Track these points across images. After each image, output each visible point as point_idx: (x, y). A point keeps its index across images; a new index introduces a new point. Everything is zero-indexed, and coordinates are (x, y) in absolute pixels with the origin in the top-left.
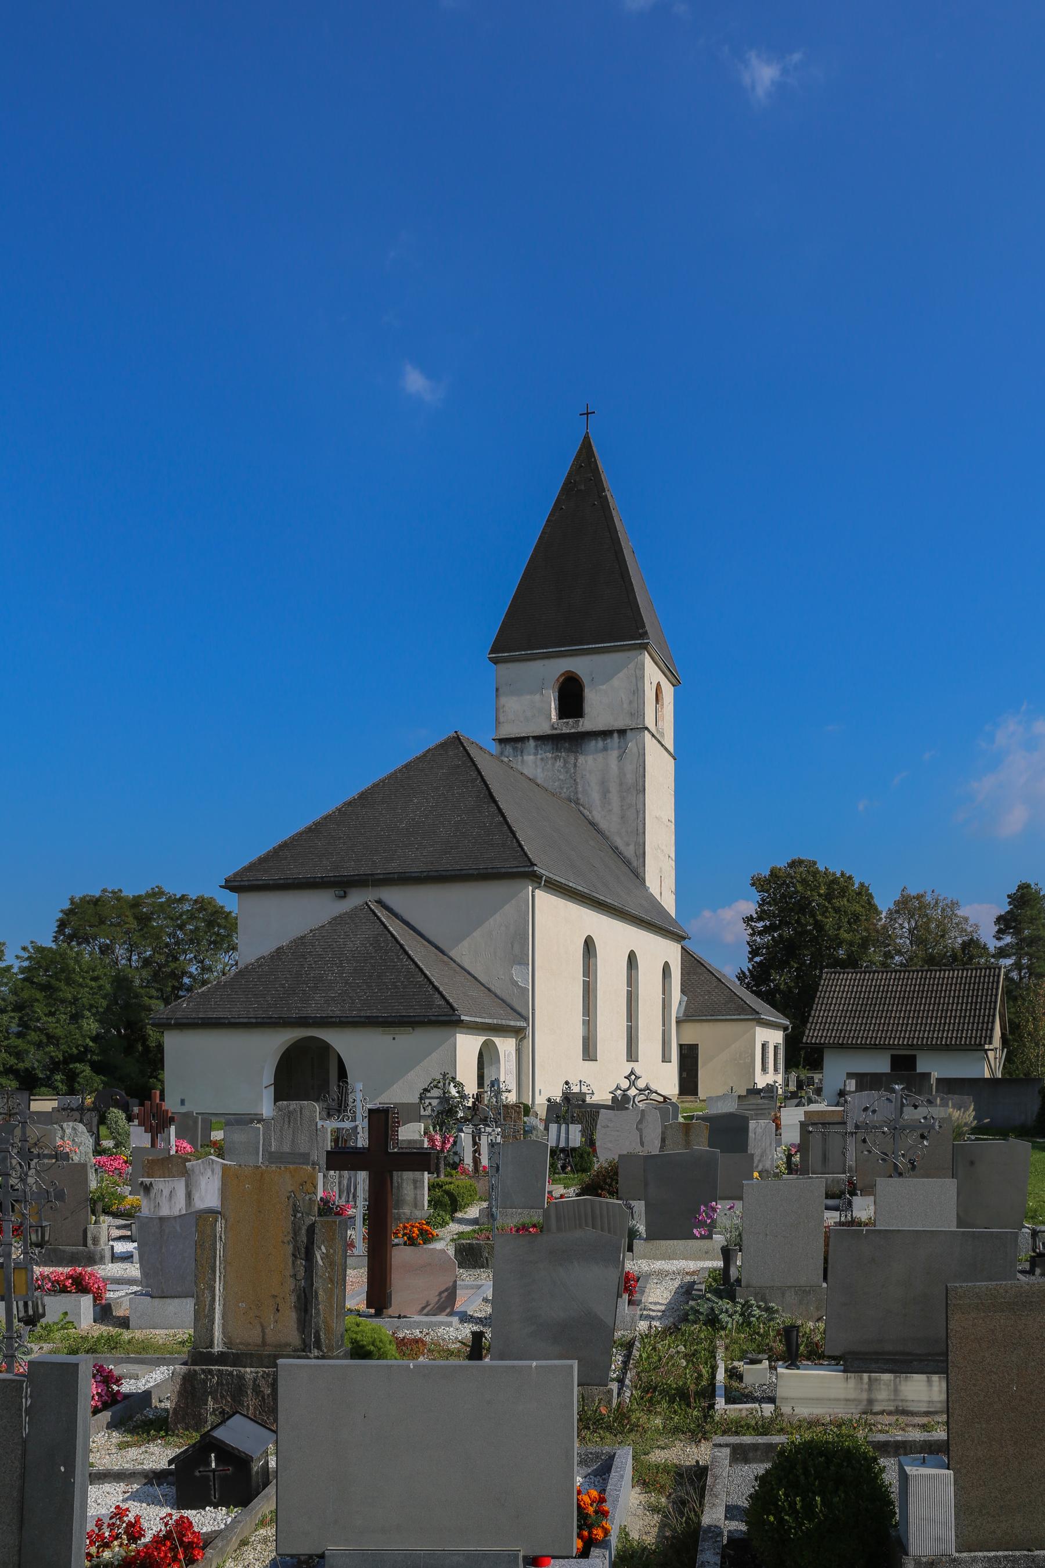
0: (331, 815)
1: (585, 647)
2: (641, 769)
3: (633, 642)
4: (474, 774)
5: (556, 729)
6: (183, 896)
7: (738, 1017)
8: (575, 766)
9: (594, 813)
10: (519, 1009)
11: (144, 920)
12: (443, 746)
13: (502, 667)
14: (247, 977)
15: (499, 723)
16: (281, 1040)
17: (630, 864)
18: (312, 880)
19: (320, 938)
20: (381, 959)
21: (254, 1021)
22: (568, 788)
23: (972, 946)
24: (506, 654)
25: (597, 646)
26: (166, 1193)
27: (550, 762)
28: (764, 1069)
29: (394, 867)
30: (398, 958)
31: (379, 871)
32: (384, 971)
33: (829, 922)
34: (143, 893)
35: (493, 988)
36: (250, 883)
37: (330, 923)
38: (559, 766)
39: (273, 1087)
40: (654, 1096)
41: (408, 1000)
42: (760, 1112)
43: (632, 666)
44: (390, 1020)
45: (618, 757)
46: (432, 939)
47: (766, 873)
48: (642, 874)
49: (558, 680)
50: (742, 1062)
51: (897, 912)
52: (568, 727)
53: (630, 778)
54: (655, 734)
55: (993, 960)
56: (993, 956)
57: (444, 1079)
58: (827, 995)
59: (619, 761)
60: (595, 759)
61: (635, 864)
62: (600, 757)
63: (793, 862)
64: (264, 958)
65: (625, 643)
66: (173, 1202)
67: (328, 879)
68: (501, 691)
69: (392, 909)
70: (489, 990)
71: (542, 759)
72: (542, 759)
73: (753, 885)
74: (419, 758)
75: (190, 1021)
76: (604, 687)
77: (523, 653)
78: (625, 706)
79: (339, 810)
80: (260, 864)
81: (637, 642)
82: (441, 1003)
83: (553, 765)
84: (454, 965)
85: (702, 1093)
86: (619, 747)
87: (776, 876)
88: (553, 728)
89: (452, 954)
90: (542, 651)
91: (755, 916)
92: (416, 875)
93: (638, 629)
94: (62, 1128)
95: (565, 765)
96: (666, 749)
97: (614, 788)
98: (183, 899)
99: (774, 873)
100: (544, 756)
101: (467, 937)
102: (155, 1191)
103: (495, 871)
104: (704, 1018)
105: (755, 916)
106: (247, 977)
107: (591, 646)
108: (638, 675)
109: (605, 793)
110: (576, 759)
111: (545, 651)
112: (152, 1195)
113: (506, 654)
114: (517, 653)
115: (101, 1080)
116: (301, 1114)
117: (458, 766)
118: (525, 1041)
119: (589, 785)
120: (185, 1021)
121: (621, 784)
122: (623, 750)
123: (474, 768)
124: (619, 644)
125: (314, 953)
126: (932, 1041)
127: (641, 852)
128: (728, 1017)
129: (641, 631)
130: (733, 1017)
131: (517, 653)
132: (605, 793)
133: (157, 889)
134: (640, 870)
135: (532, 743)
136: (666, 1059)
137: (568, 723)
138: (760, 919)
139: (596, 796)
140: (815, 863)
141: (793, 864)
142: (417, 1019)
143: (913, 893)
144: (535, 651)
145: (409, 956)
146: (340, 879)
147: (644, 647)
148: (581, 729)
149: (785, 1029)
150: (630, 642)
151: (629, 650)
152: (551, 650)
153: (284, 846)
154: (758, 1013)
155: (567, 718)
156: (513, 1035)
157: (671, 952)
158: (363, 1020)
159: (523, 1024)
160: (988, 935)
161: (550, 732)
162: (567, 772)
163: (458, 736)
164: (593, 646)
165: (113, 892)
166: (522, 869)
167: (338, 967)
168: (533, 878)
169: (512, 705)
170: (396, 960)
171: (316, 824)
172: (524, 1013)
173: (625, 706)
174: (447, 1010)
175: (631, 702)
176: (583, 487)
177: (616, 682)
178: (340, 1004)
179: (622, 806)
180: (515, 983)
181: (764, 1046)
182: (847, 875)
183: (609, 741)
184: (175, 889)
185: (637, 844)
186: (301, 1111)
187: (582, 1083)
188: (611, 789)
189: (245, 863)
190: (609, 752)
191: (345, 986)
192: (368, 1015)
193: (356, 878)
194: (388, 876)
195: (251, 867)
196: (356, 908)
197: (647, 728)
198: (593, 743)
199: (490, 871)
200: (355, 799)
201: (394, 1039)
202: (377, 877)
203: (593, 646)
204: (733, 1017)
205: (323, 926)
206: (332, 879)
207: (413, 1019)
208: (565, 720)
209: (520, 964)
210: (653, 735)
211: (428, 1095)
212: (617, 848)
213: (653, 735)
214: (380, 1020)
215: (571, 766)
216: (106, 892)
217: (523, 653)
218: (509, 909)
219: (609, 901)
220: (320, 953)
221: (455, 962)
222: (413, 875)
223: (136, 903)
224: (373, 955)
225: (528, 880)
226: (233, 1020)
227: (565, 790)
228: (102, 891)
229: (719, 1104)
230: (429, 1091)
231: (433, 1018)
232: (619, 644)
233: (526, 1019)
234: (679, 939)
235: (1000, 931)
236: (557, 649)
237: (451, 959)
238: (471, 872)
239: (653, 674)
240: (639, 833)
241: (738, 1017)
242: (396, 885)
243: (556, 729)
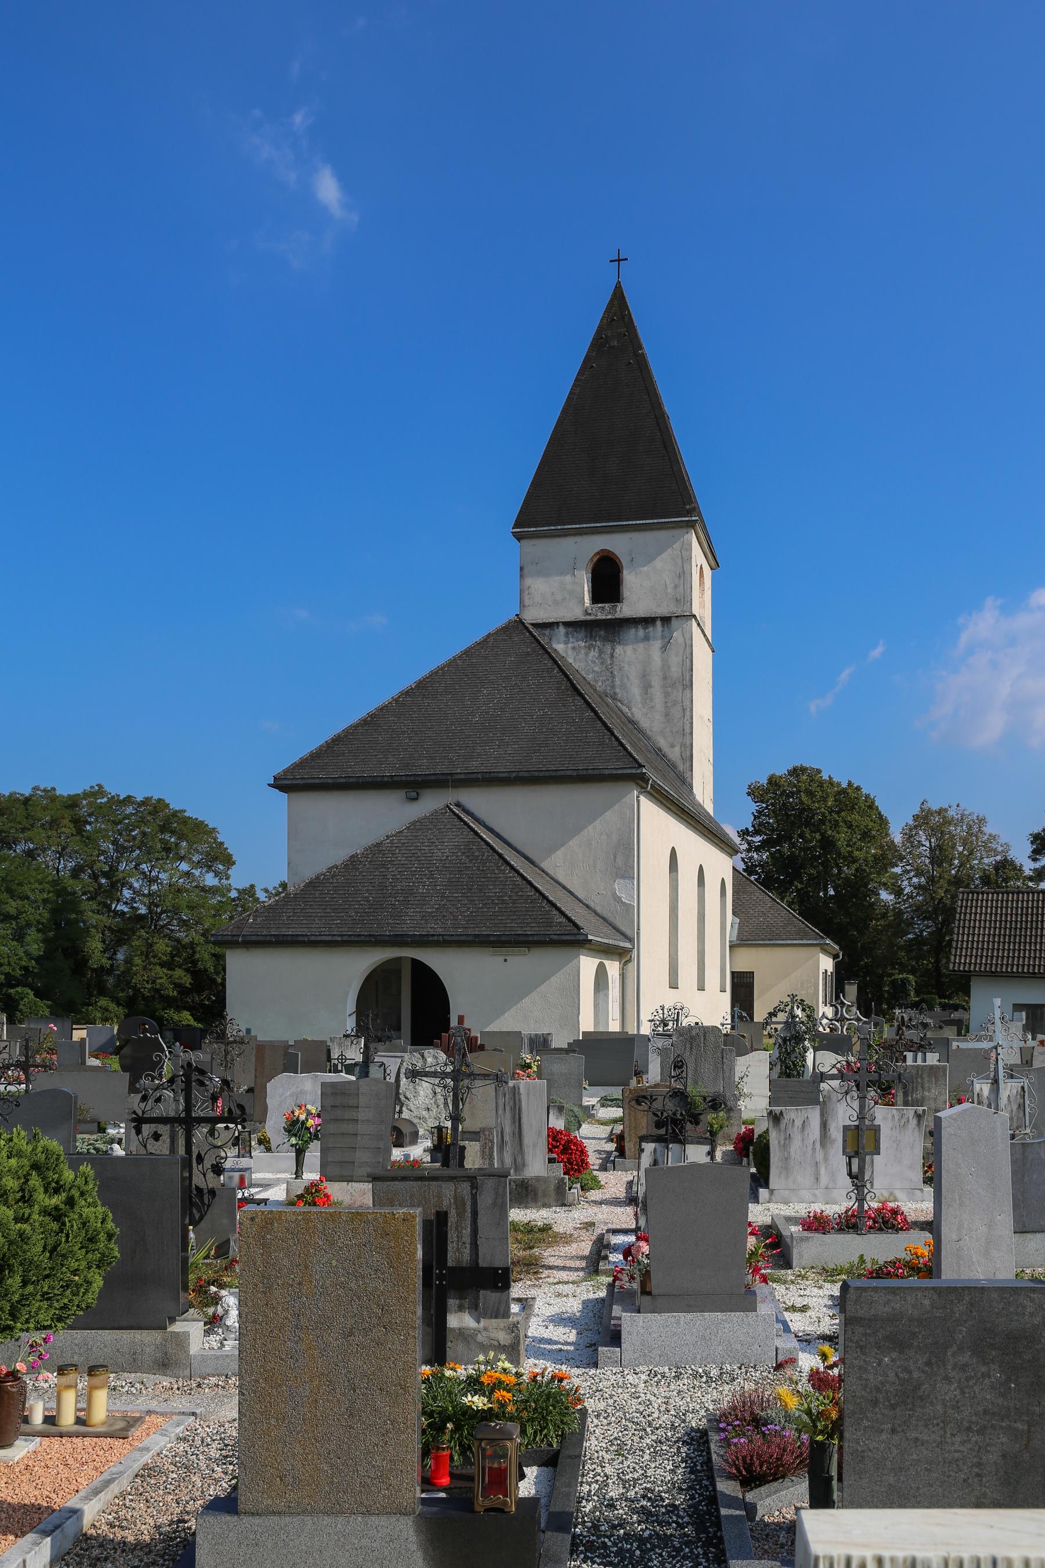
0: (387, 706)
1: (624, 523)
3: (679, 519)
4: (550, 663)
5: (590, 614)
6: (129, 797)
7: (801, 942)
8: (612, 656)
9: (634, 709)
10: (623, 929)
11: (79, 823)
13: (525, 542)
14: (320, 888)
15: (524, 606)
16: (362, 963)
17: (675, 767)
18: (379, 779)
19: (400, 845)
20: (478, 869)
21: (339, 939)
22: (603, 682)
23: (1006, 867)
24: (532, 529)
25: (638, 522)
26: (798, 1123)
27: (583, 652)
29: (475, 766)
30: (498, 868)
31: (459, 771)
32: (486, 883)
33: (842, 838)
34: (80, 791)
35: (592, 904)
36: (304, 781)
37: (408, 828)
38: (594, 656)
39: (354, 1016)
41: (522, 917)
43: (677, 546)
44: (503, 939)
45: (661, 648)
46: (519, 847)
47: (764, 781)
48: (689, 779)
49: (591, 559)
50: (804, 992)
51: (915, 827)
52: (603, 612)
53: (675, 671)
55: (1030, 884)
56: (1031, 879)
57: (792, 1002)
58: (968, 917)
59: (663, 653)
60: (635, 650)
61: (681, 767)
62: (641, 646)
63: (795, 769)
64: (336, 867)
65: (670, 520)
66: (806, 1132)
67: (399, 779)
68: (526, 571)
69: (473, 814)
70: (588, 906)
71: (574, 648)
72: (574, 648)
73: (749, 794)
74: (479, 644)
75: (260, 938)
76: (646, 568)
77: (552, 528)
78: (669, 590)
79: (396, 700)
80: (312, 760)
81: (684, 519)
82: (561, 920)
83: (587, 654)
84: (548, 878)
86: (663, 637)
87: (776, 784)
88: (587, 613)
89: (543, 865)
90: (574, 526)
91: (751, 829)
92: (504, 775)
93: (684, 504)
94: (423, 1056)
95: (600, 655)
96: (705, 635)
97: (656, 682)
98: (129, 800)
99: (773, 781)
100: (576, 644)
101: (563, 845)
102: (786, 1121)
103: (596, 772)
104: (761, 942)
105: (751, 829)
106: (320, 888)
107: (631, 523)
108: (684, 556)
109: (646, 687)
110: (613, 649)
111: (578, 526)
112: (782, 1126)
113: (532, 529)
114: (546, 528)
115: (45, 1004)
116: (705, 1039)
117: (528, 654)
118: (630, 965)
119: (628, 679)
120: (254, 938)
121: (665, 678)
122: (666, 640)
123: (546, 656)
124: (663, 520)
125: (397, 862)
126: (980, 968)
127: (688, 754)
128: (789, 942)
129: (688, 507)
131: (546, 528)
132: (646, 687)
133: (97, 788)
134: (687, 775)
136: (723, 990)
137: (603, 608)
138: (757, 832)
139: (635, 691)
140: (819, 771)
141: (795, 772)
142: (535, 938)
143: (935, 807)
144: (566, 527)
145: (512, 867)
146: (412, 779)
147: (691, 525)
148: (618, 615)
150: (676, 519)
151: (674, 528)
152: (585, 526)
153: (337, 740)
155: (602, 603)
156: (617, 957)
158: (470, 938)
159: (628, 945)
160: (1021, 854)
161: (582, 618)
162: (602, 663)
163: (521, 620)
164: (634, 522)
165: (45, 790)
166: (629, 771)
167: (429, 878)
168: (640, 782)
169: (539, 586)
170: (496, 871)
171: (372, 716)
172: (628, 932)
173: (669, 590)
174: (570, 928)
175: (676, 587)
176: (616, 343)
177: (658, 563)
178: (440, 920)
179: (666, 702)
180: (618, 900)
182: (855, 786)
183: (651, 629)
184: (118, 788)
185: (683, 745)
186: (705, 1036)
188: (653, 683)
189: (295, 758)
190: (652, 642)
191: (442, 900)
192: (477, 933)
193: (433, 778)
194: (471, 776)
195: (302, 764)
196: (436, 812)
197: (694, 616)
198: (633, 631)
199: (590, 772)
200: (412, 689)
201: (506, 960)
202: (457, 777)
203: (634, 522)
205: (401, 832)
206: (404, 778)
207: (531, 938)
208: (600, 605)
209: (623, 877)
211: (774, 1019)
212: (660, 750)
214: (492, 939)
215: (607, 657)
216: (38, 790)
217: (552, 528)
218: (611, 816)
220: (403, 862)
221: (547, 874)
222: (501, 775)
223: (72, 803)
224: (468, 865)
226: (313, 938)
227: (600, 684)
228: (34, 788)
230: (776, 1016)
231: (555, 937)
232: (663, 520)
233: (630, 940)
234: (730, 851)
235: (1035, 852)
236: (592, 525)
237: (543, 871)
238: (568, 773)
239: (698, 557)
240: (687, 733)
241: (801, 942)
242: (479, 786)
243: (590, 614)
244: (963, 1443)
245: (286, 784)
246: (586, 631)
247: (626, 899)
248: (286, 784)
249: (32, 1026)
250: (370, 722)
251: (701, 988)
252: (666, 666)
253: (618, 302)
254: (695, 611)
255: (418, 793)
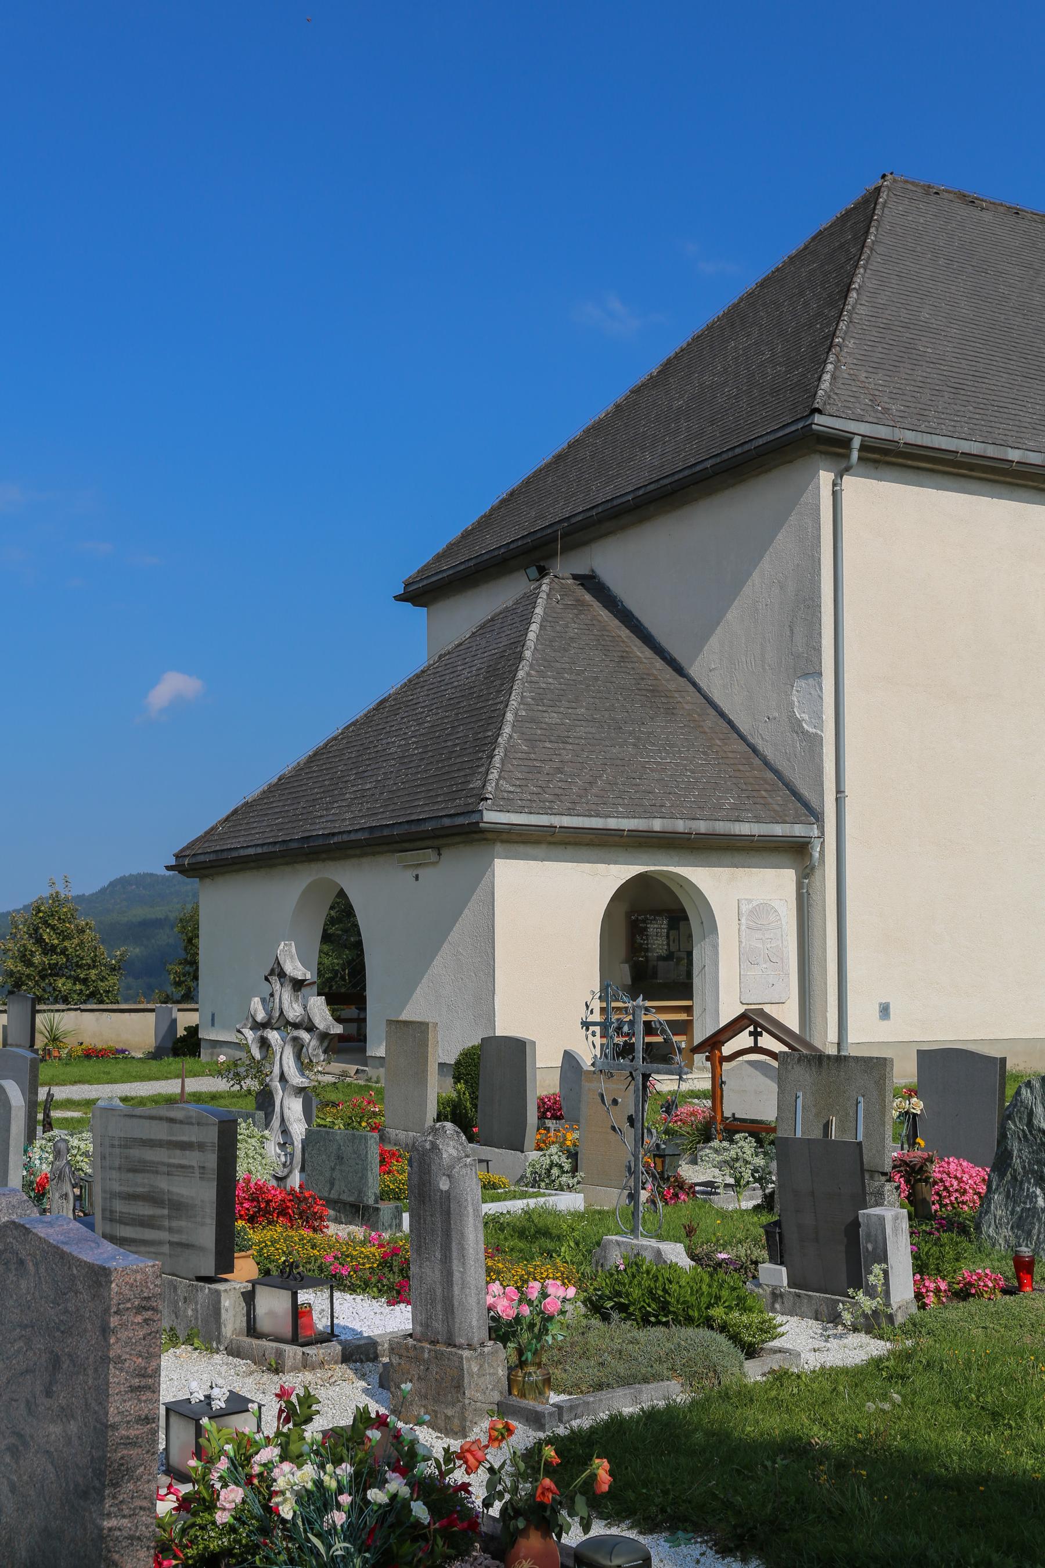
172: (814, 803)
180: (796, 726)
209: (806, 675)
233: (816, 816)
247: (810, 723)
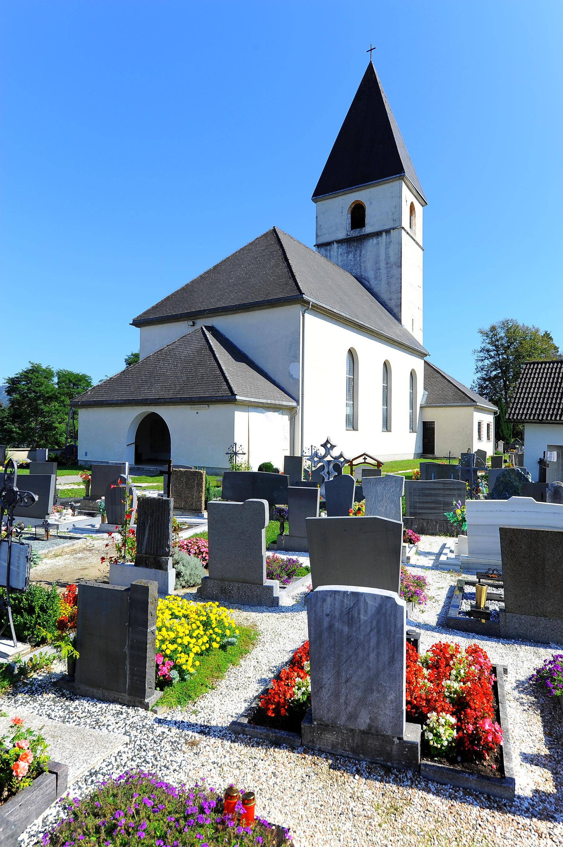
2: (400, 254)
8: (360, 256)
12: (266, 235)
28: (480, 438)
40: (369, 460)
42: (448, 492)
52: (356, 233)
54: (409, 232)
83: (347, 257)
85: (437, 453)
96: (417, 243)
97: (383, 265)
121: (387, 264)
128: (455, 404)
130: (458, 404)
135: (335, 245)
149: (495, 413)
154: (474, 401)
157: (418, 365)
181: (479, 424)
183: (380, 238)
187: (313, 448)
197: (403, 228)
204: (458, 404)
210: (408, 233)
213: (408, 233)
219: (367, 325)
225: (300, 305)
229: (378, 488)
233: (298, 402)
244: (488, 701)
245: (138, 323)
246: (347, 244)
248: (138, 323)
249: (411, 471)
250: (184, 290)
251: (387, 425)
252: (387, 257)
253: (370, 72)
254: (403, 225)
255: (193, 323)
